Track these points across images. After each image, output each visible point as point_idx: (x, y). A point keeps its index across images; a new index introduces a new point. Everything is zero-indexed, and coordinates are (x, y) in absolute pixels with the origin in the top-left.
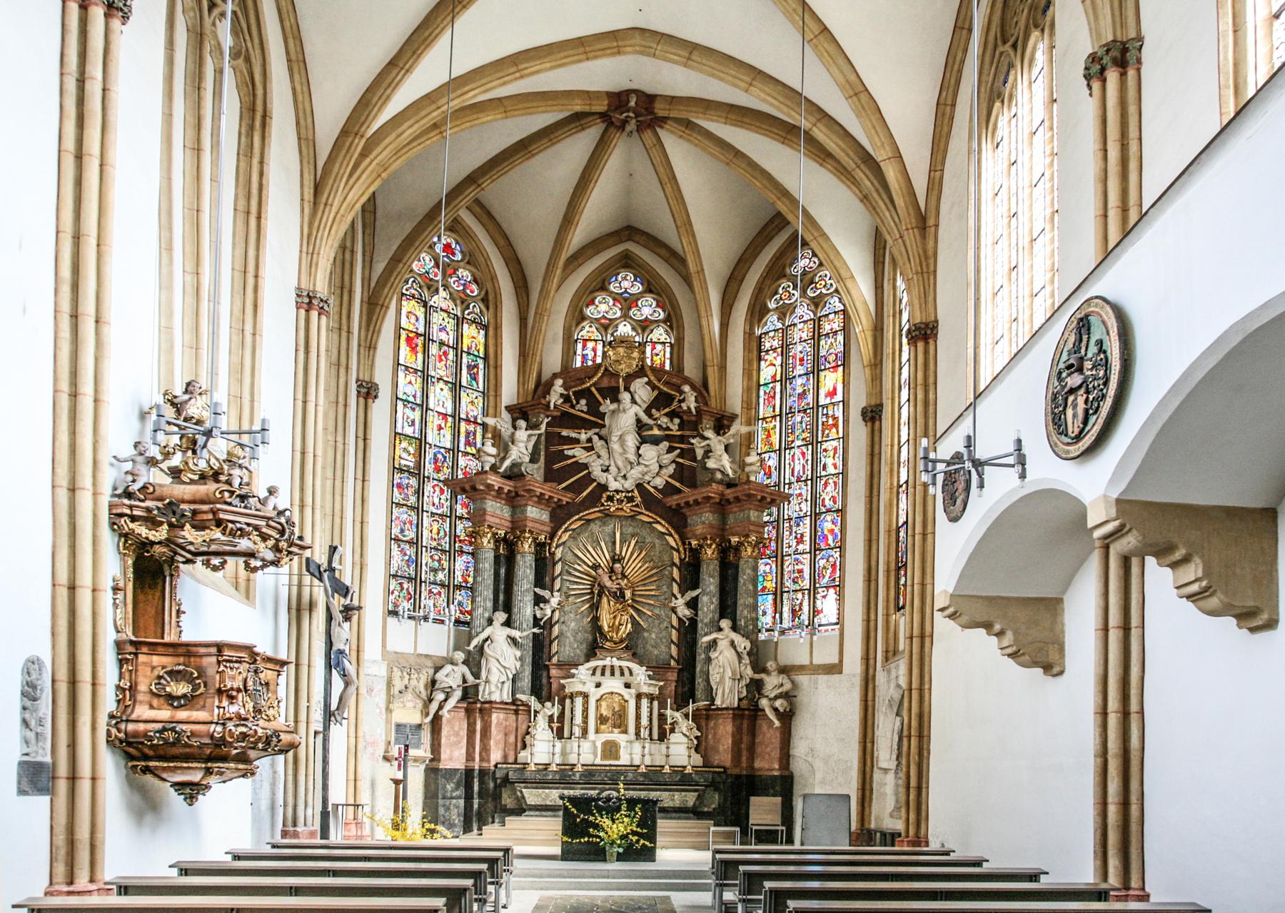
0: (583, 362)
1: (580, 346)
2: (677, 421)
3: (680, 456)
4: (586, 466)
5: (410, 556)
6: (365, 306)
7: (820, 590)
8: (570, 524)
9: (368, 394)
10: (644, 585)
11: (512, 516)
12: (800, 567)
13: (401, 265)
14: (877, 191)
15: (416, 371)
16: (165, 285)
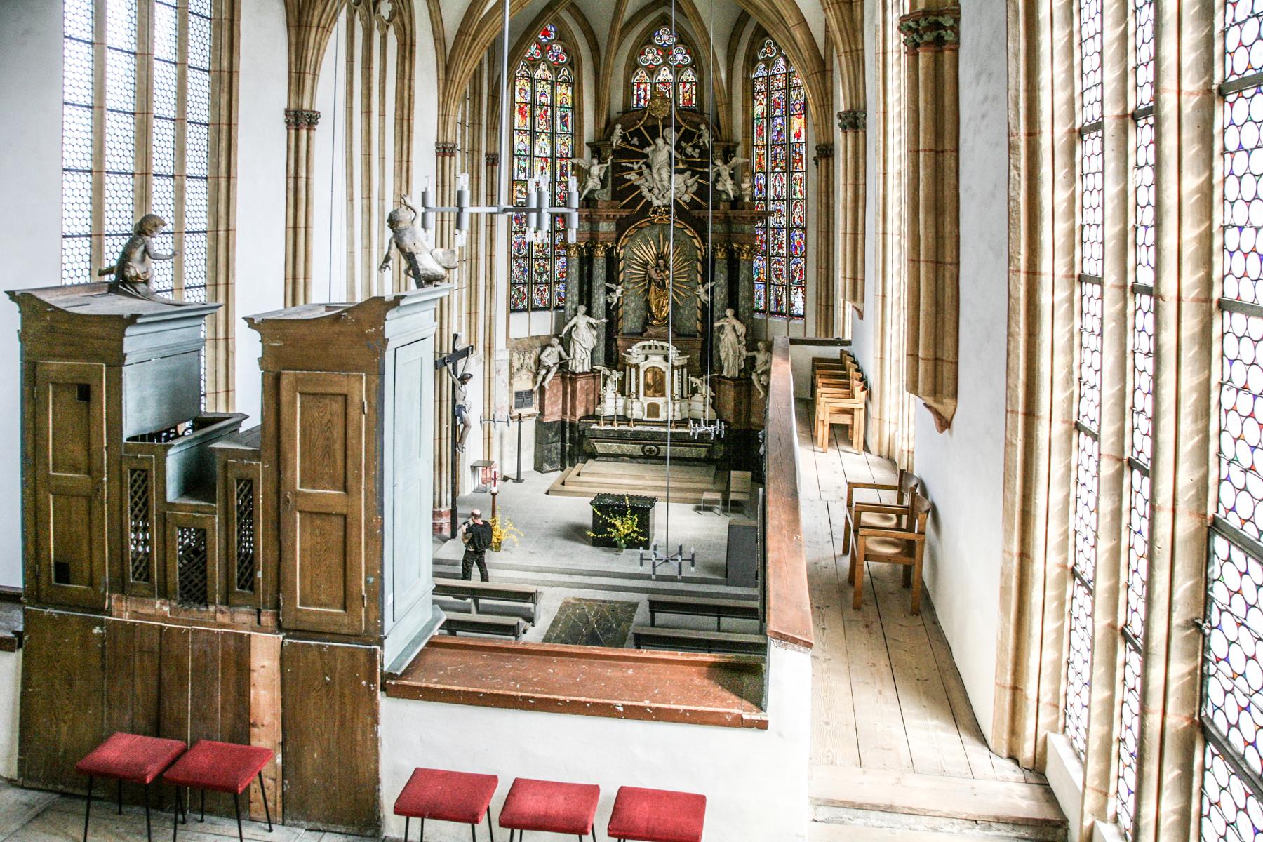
1: (635, 88)
2: (697, 151)
4: (638, 187)
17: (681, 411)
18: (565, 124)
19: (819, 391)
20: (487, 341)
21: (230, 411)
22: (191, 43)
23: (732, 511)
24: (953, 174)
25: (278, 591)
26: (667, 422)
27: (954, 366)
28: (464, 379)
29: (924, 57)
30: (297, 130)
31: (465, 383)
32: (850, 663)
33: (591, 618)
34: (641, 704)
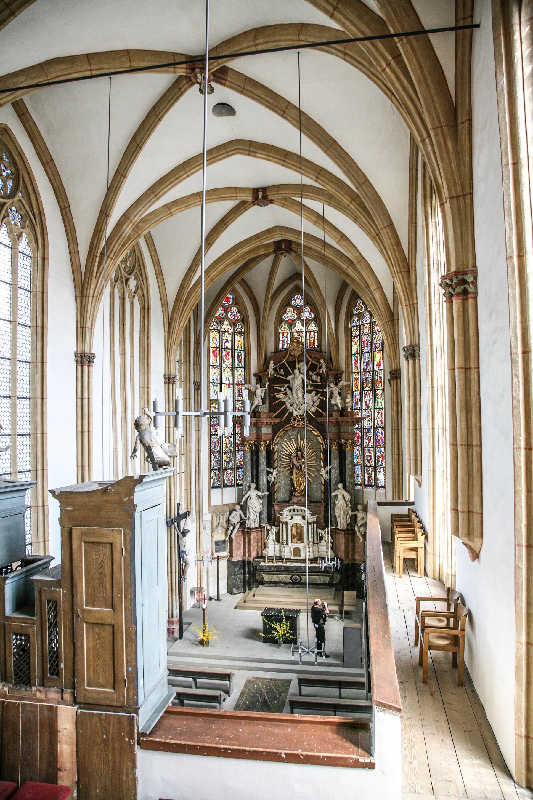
1: (281, 336)
2: (319, 377)
3: (320, 396)
4: (284, 403)
6: (196, 344)
7: (378, 468)
9: (198, 388)
12: (370, 454)
17: (313, 552)
18: (241, 362)
19: (396, 536)
20: (198, 508)
21: (47, 554)
22: (19, 308)
23: (345, 618)
24: (476, 384)
25: (74, 676)
26: (305, 559)
27: (480, 515)
28: (184, 533)
29: (456, 303)
30: (82, 366)
31: (185, 536)
32: (422, 720)
33: (264, 691)
34: (296, 752)
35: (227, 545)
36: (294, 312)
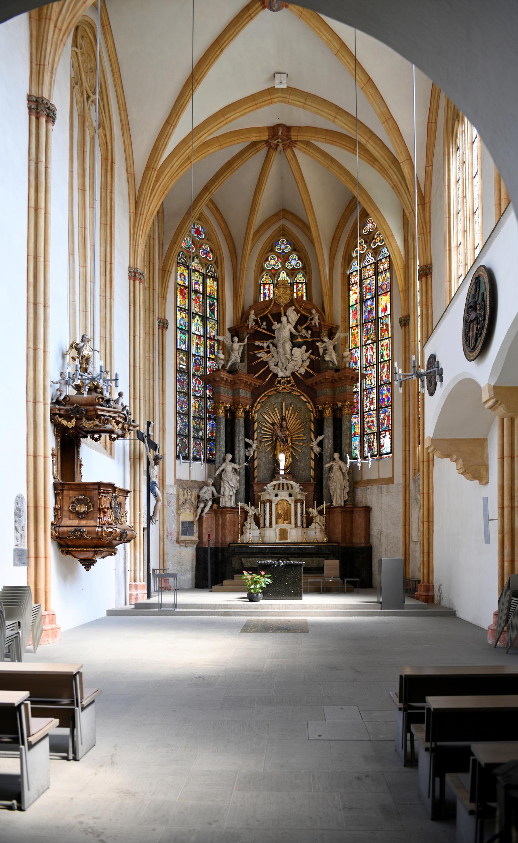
0: (264, 298)
1: (262, 287)
2: (310, 332)
4: (266, 363)
5: (186, 423)
6: (161, 271)
8: (261, 399)
10: (297, 434)
11: (233, 396)
13: (176, 245)
14: (400, 182)
15: (185, 310)
16: (71, 277)
18: (212, 311)
30: (37, 118)
35: (196, 529)
36: (278, 260)
